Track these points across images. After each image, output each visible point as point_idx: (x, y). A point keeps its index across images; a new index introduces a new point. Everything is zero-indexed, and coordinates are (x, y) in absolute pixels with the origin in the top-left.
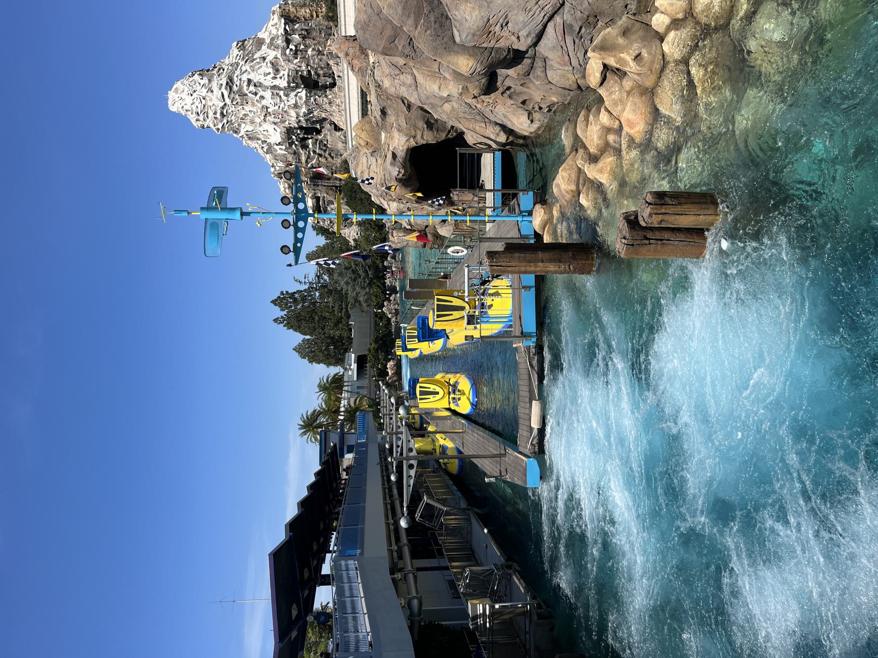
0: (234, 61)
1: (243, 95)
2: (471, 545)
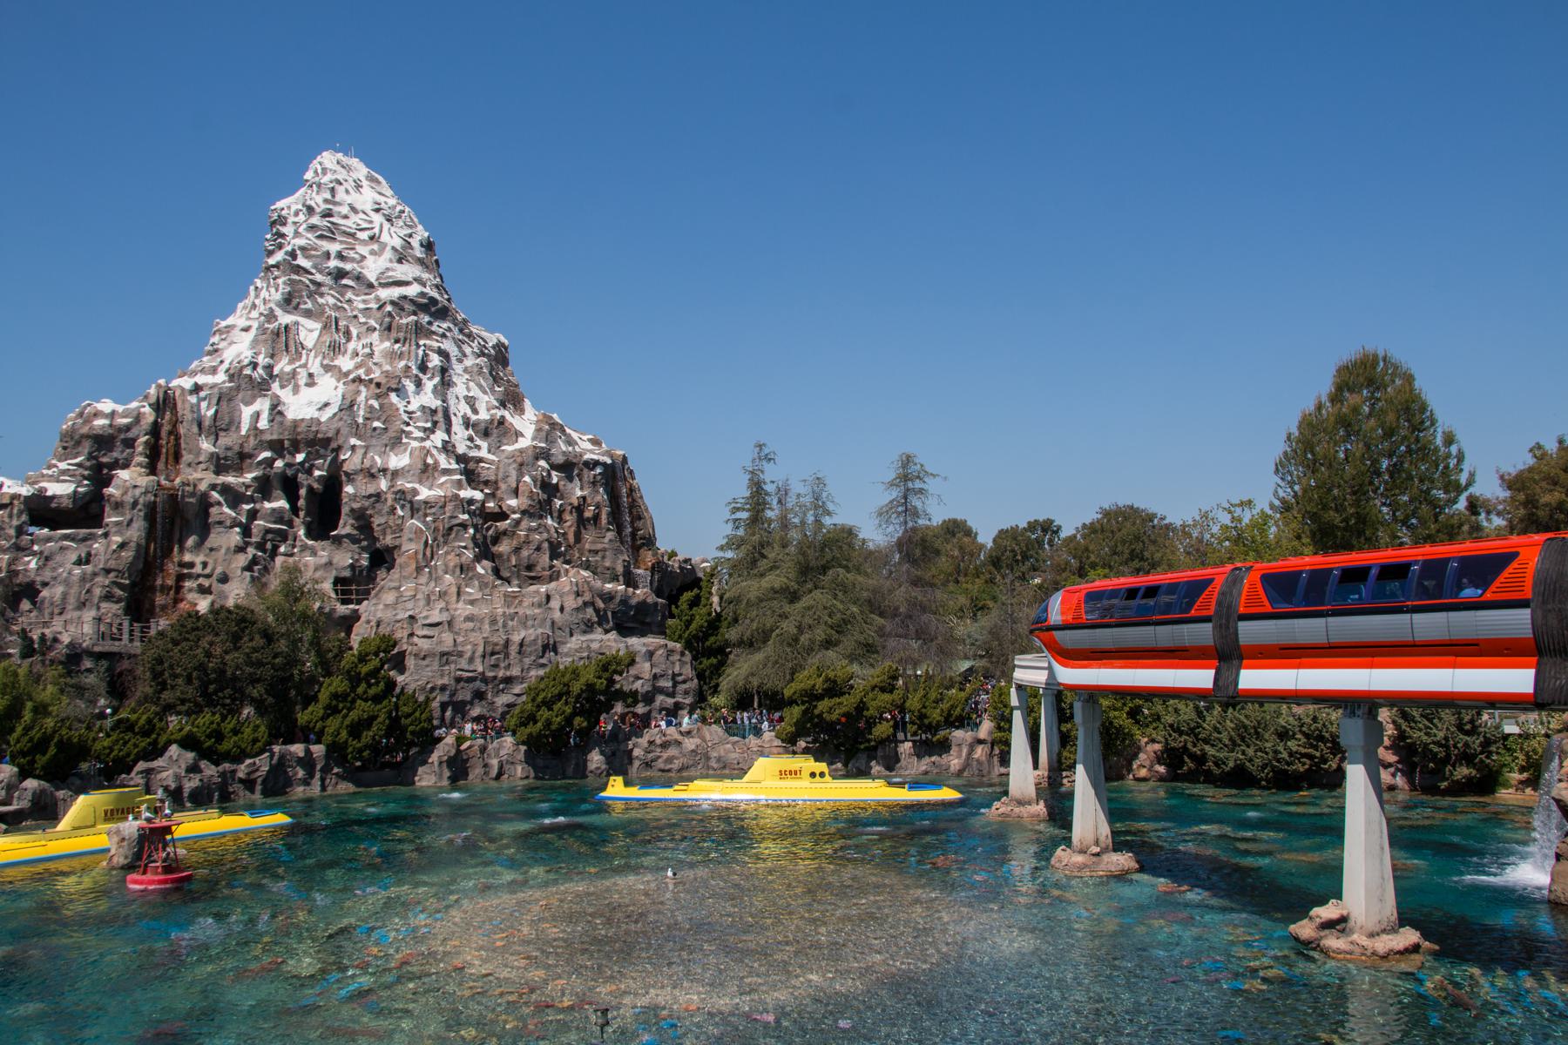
1: (420, 331)
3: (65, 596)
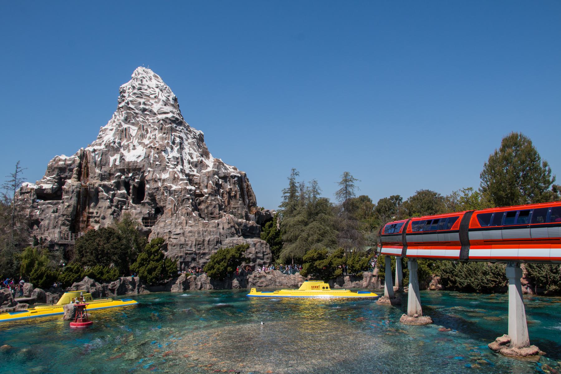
1: (172, 130)
2: (419, 282)
3: (49, 224)
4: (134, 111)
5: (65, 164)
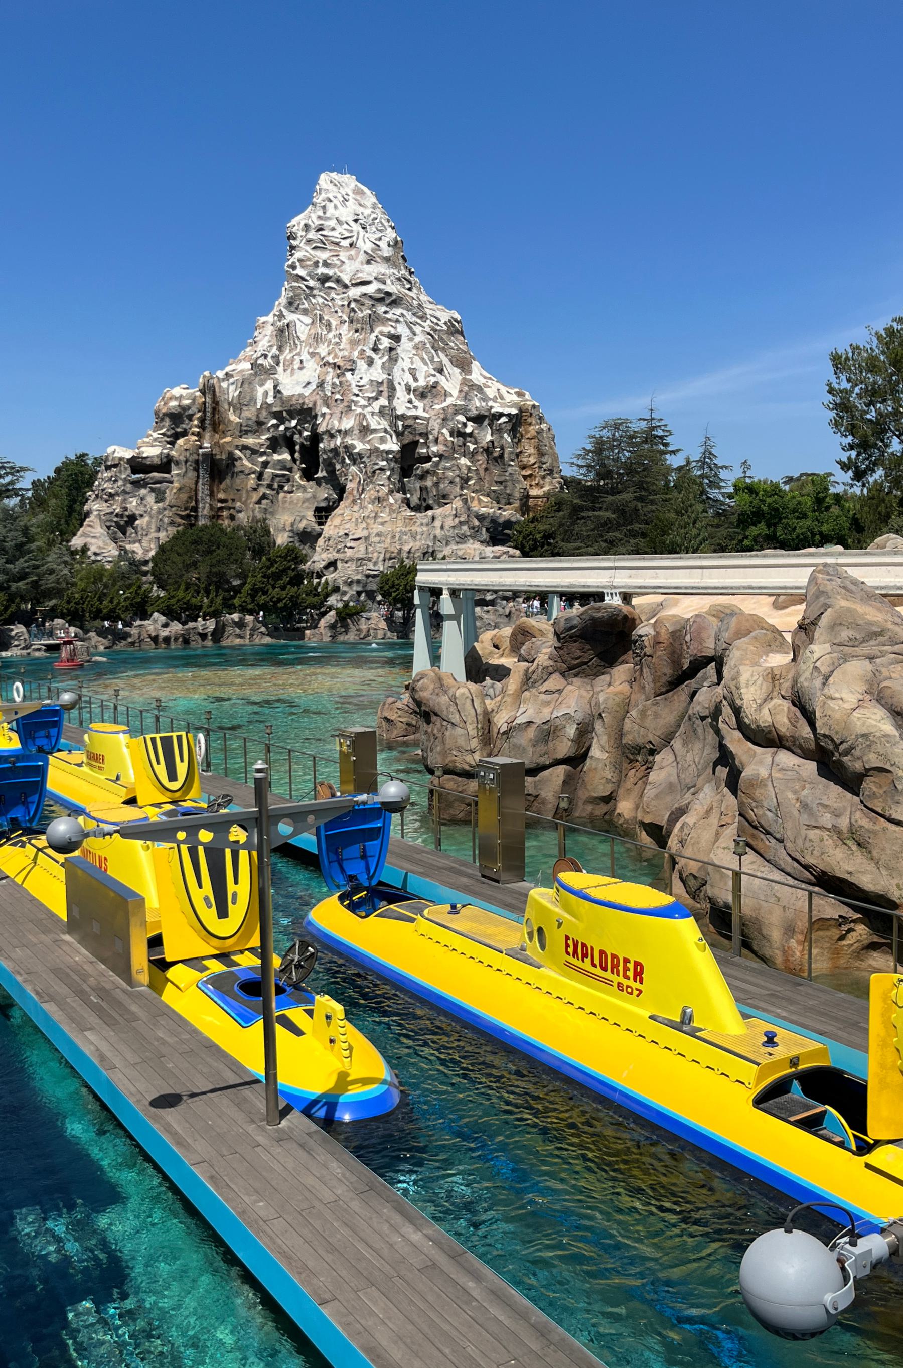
0: (428, 312)
1: (373, 320)
3: (149, 523)
4: (306, 283)
5: (179, 406)
